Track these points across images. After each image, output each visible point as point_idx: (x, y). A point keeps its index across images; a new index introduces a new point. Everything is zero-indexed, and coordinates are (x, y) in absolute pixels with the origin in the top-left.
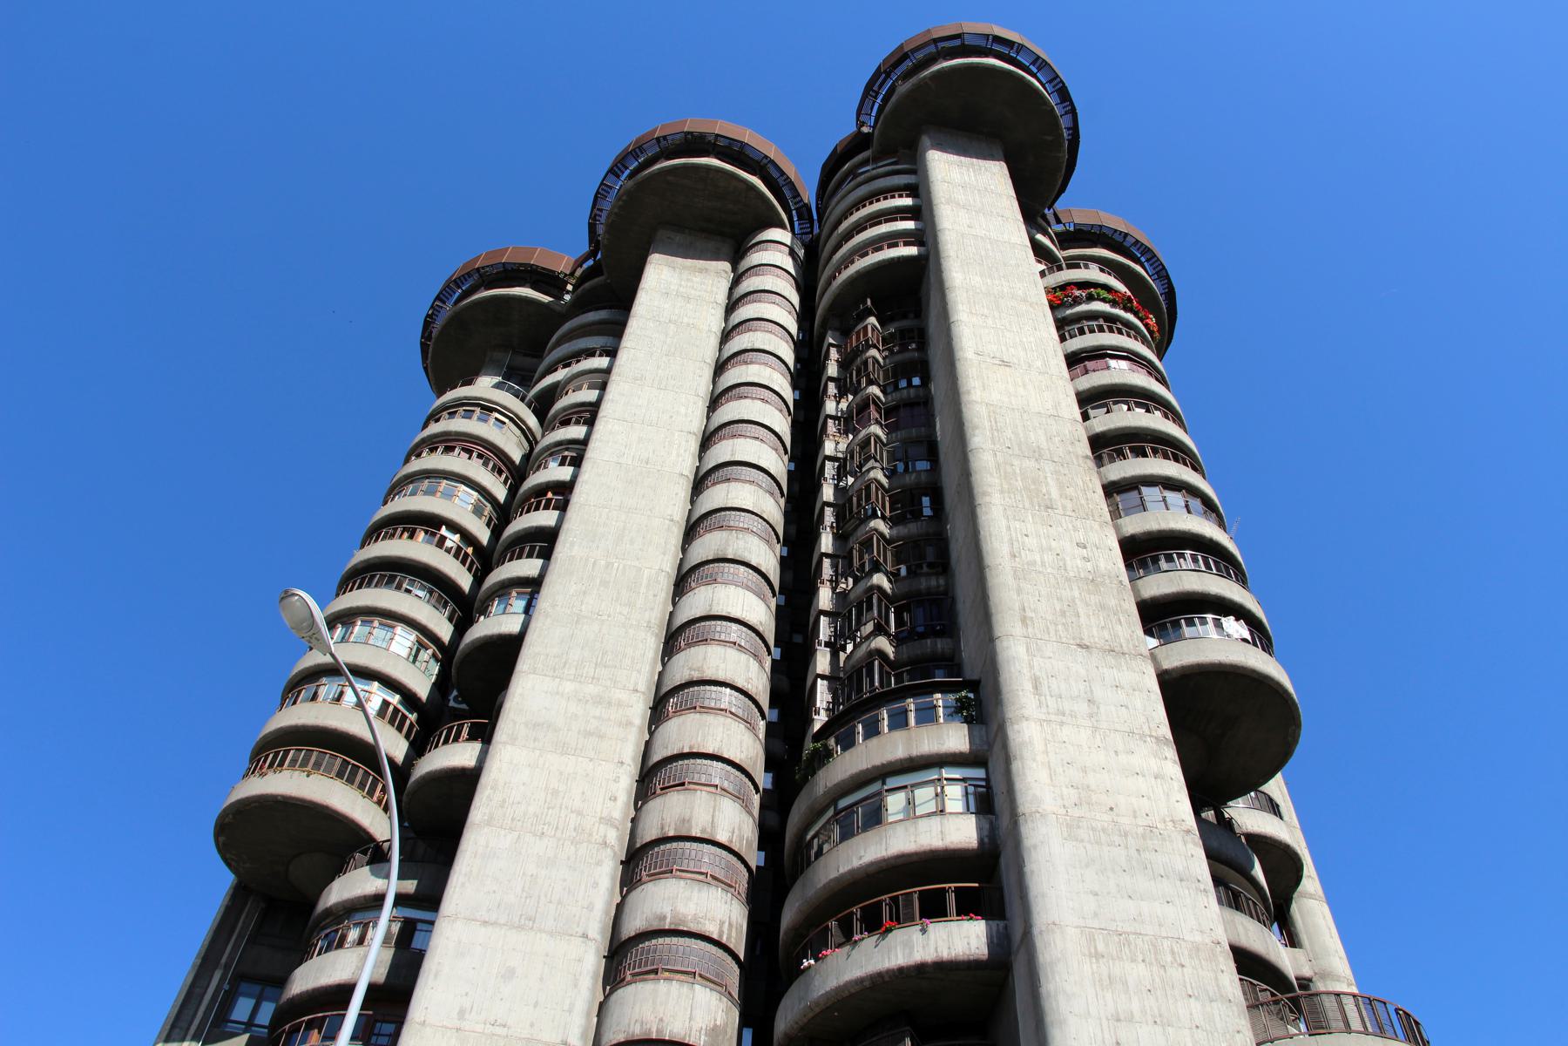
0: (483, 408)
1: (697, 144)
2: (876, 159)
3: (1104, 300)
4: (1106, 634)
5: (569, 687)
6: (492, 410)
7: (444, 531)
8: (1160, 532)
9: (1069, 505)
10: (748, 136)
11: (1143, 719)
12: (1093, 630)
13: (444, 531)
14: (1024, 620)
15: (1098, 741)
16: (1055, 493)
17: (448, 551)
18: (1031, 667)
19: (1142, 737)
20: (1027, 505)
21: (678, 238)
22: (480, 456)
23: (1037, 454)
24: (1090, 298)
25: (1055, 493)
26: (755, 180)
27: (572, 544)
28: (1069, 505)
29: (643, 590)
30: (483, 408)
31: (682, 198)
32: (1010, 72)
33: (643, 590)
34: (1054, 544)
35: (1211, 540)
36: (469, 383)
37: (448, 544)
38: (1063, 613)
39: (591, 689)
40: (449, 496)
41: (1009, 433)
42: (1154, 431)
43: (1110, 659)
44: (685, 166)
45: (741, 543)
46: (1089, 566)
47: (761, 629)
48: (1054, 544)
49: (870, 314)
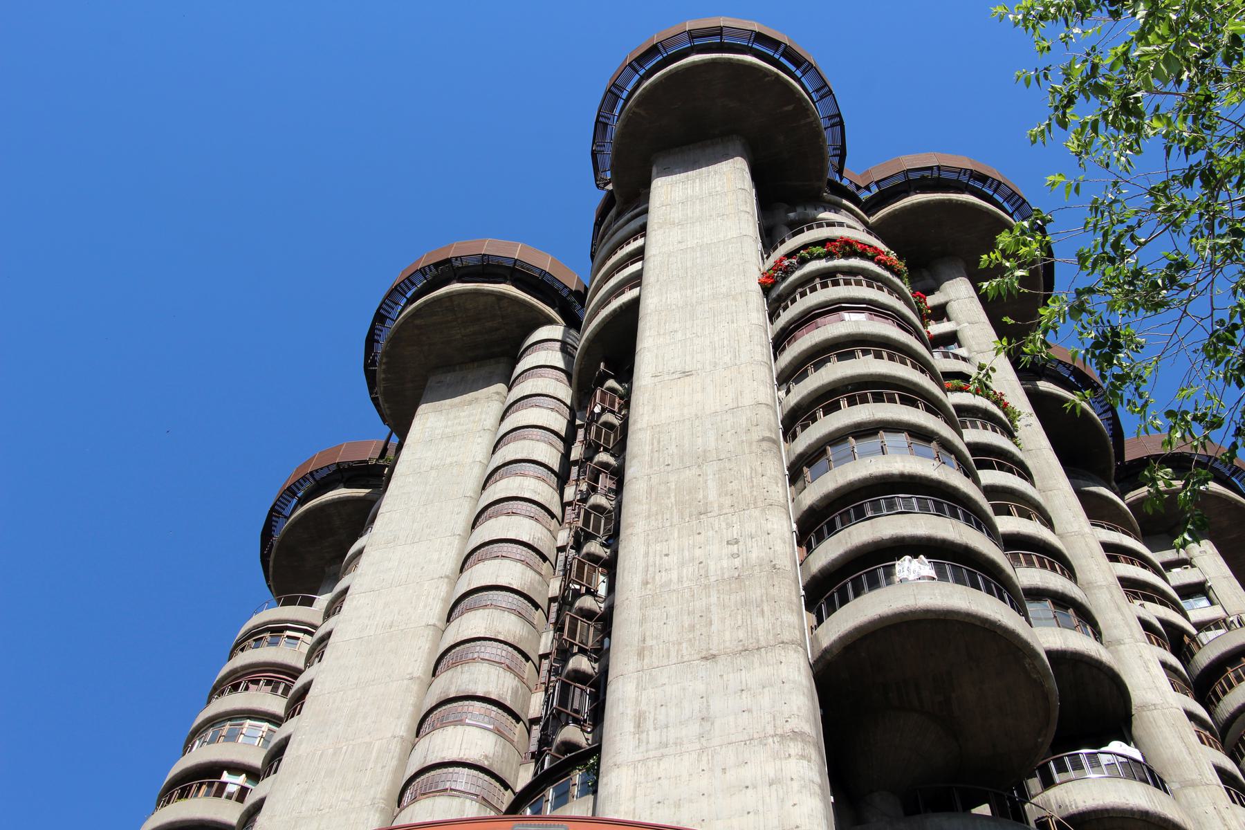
0: (273, 630)
1: (447, 270)
2: (619, 215)
3: (819, 257)
4: (741, 634)
6: (282, 630)
7: (226, 777)
8: (837, 490)
9: (727, 501)
10: (493, 246)
11: (768, 718)
13: (226, 777)
14: (641, 654)
15: (704, 765)
16: (712, 495)
17: (229, 797)
18: (638, 702)
19: (762, 741)
20: (676, 520)
21: (449, 378)
22: (268, 683)
24: (803, 261)
25: (712, 495)
26: (456, 287)
27: (300, 743)
29: (371, 765)
30: (273, 630)
31: (442, 336)
32: (714, 61)
33: (371, 765)
34: (698, 552)
35: (902, 476)
36: (1153, 551)
37: (231, 788)
38: (692, 628)
40: (232, 737)
41: (673, 449)
42: (852, 377)
43: (741, 661)
44: (426, 304)
45: (466, 677)
46: (737, 562)
47: (486, 764)
49: (608, 377)
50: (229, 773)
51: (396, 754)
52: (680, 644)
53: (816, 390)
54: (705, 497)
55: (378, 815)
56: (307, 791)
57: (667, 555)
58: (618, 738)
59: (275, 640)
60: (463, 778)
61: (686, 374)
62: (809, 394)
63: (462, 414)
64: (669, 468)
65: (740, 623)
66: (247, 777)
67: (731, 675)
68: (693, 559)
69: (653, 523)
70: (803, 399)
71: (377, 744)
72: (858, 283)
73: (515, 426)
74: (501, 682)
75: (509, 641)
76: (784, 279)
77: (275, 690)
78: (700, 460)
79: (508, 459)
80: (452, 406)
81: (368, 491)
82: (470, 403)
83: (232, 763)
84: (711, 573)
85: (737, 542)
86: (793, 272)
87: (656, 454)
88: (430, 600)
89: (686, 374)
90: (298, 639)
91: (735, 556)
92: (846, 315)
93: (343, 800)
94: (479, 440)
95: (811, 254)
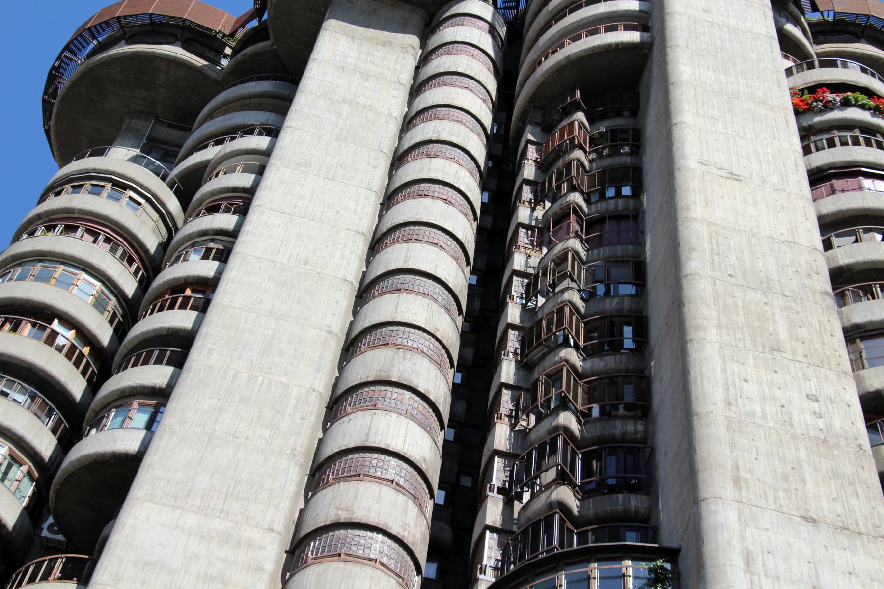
0: (116, 184)
3: (863, 107)
5: (191, 520)
6: (125, 187)
7: (56, 325)
9: (800, 349)
12: (823, 500)
13: (56, 325)
14: (737, 481)
17: (60, 349)
18: (743, 538)
23: (765, 286)
24: (846, 104)
25: (783, 334)
27: (211, 352)
28: (800, 349)
29: (289, 411)
30: (116, 184)
33: (289, 411)
37: (60, 341)
39: (217, 524)
41: (733, 259)
43: (842, 538)
45: (408, 365)
46: (821, 423)
48: (778, 394)
49: (578, 108)
50: (60, 322)
51: (315, 410)
52: (776, 490)
53: (873, 262)
54: (776, 332)
55: (297, 469)
56: (220, 410)
57: (746, 381)
58: (729, 569)
59: (116, 194)
60: (65, 336)
61: (734, 177)
62: (865, 263)
63: (377, 53)
64: (733, 280)
65: (835, 494)
66: (77, 333)
67: (836, 551)
68: (774, 399)
69: (725, 336)
70: (857, 264)
71: (295, 391)
72: (856, 142)
73: (449, 102)
74: (438, 384)
75: (445, 342)
76: (821, 112)
77: (113, 251)
78: (764, 286)
79: (444, 137)
80: (366, 39)
81: (205, 63)
82: (384, 44)
83: (66, 314)
84: (795, 423)
85: (817, 401)
86: (832, 110)
87: (716, 258)
88: (347, 253)
89: (734, 177)
90: (139, 204)
91: (818, 415)
92: (867, 183)
93: (260, 437)
94: (395, 93)
95: (856, 100)
